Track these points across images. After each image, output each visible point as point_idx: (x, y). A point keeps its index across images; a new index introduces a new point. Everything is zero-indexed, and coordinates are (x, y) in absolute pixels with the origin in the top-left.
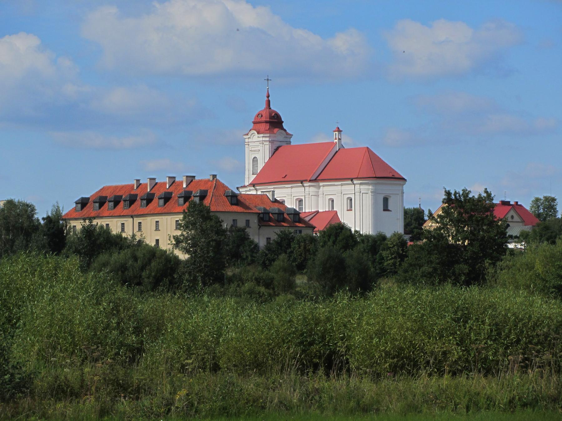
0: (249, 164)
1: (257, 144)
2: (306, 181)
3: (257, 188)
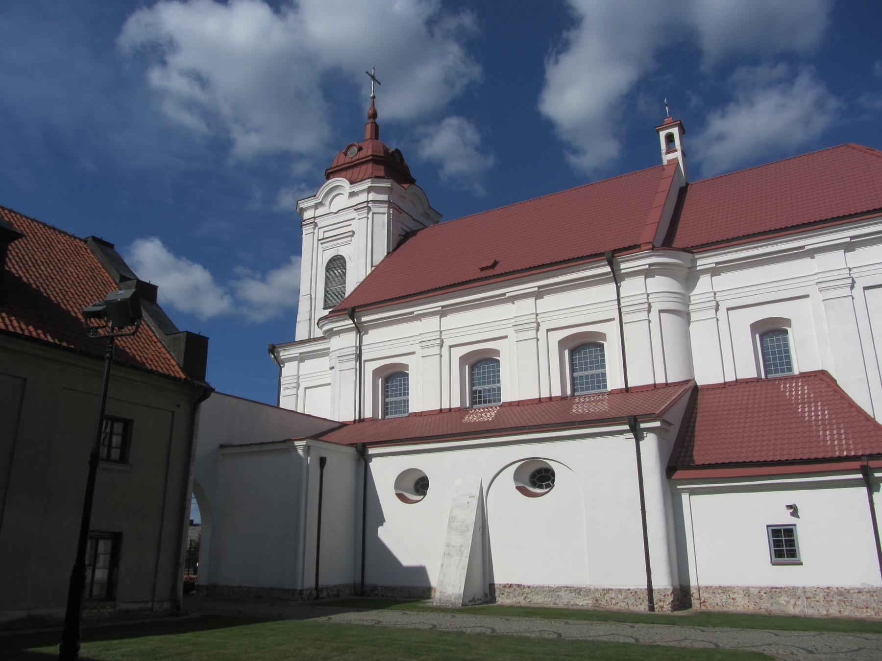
0: (313, 279)
1: (352, 214)
2: (632, 248)
3: (364, 319)
